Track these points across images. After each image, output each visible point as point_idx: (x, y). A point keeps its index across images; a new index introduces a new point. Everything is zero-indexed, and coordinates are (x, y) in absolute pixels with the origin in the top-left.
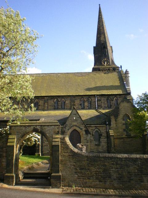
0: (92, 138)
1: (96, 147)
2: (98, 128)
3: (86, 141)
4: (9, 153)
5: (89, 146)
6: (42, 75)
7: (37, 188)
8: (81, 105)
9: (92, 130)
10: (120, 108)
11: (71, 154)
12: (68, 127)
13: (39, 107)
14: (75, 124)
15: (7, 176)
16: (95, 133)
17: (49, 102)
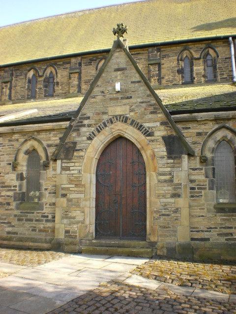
0: (203, 178)
1: (219, 218)
2: (230, 124)
3: (168, 189)
5: (185, 212)
6: (81, 14)
8: (181, 71)
9: (199, 134)
12: (89, 126)
13: (56, 88)
14: (119, 110)
16: (213, 150)
17: (83, 71)
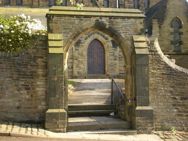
4: (54, 68)
5: (118, 65)
7: (121, 134)
10: (168, 7)
11: (165, 73)
15: (49, 114)
